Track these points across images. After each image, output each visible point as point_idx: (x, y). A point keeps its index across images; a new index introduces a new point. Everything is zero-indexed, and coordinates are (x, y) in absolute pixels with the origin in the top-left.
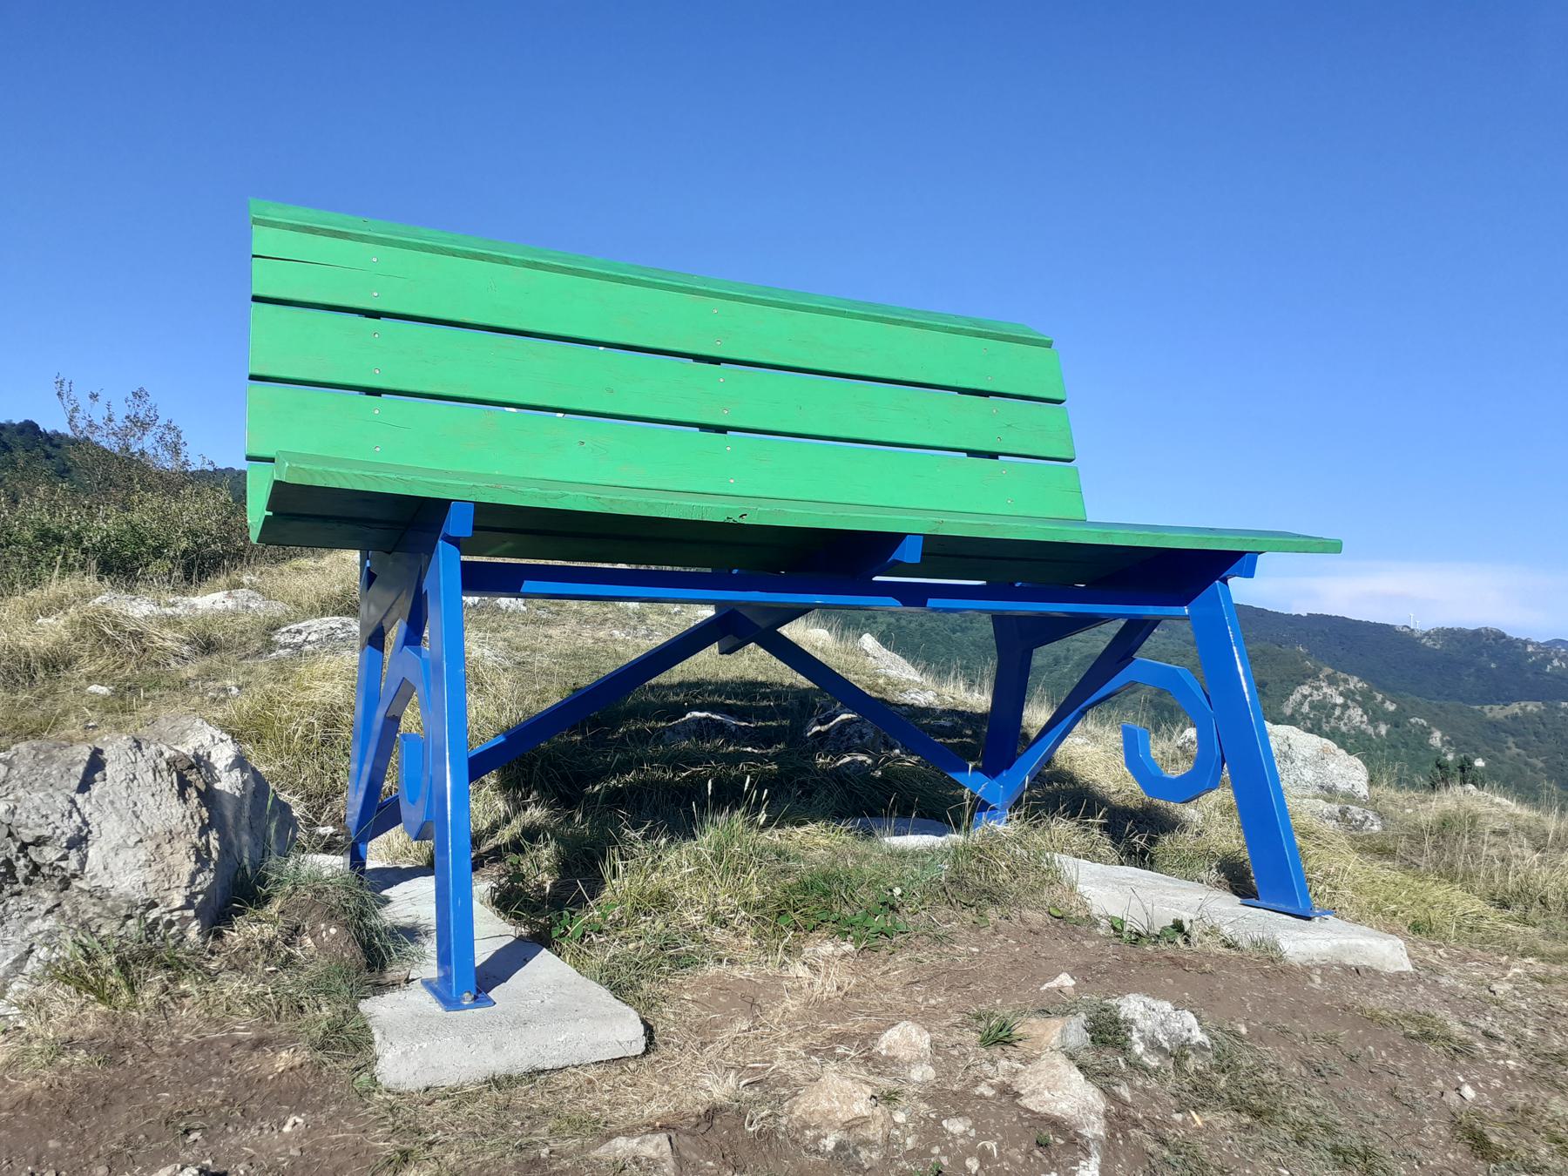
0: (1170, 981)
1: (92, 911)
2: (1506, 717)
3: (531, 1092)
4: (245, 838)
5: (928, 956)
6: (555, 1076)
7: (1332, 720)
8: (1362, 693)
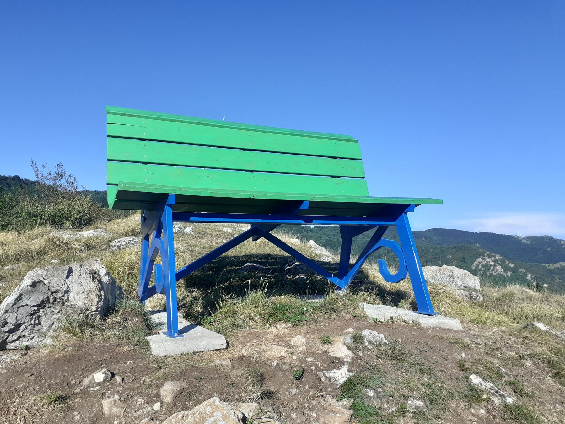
0: (383, 330)
1: (70, 312)
2: (555, 268)
3: (194, 357)
4: (110, 296)
5: (313, 326)
6: (201, 353)
7: (490, 271)
8: (501, 261)
